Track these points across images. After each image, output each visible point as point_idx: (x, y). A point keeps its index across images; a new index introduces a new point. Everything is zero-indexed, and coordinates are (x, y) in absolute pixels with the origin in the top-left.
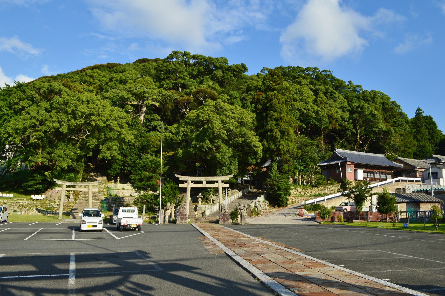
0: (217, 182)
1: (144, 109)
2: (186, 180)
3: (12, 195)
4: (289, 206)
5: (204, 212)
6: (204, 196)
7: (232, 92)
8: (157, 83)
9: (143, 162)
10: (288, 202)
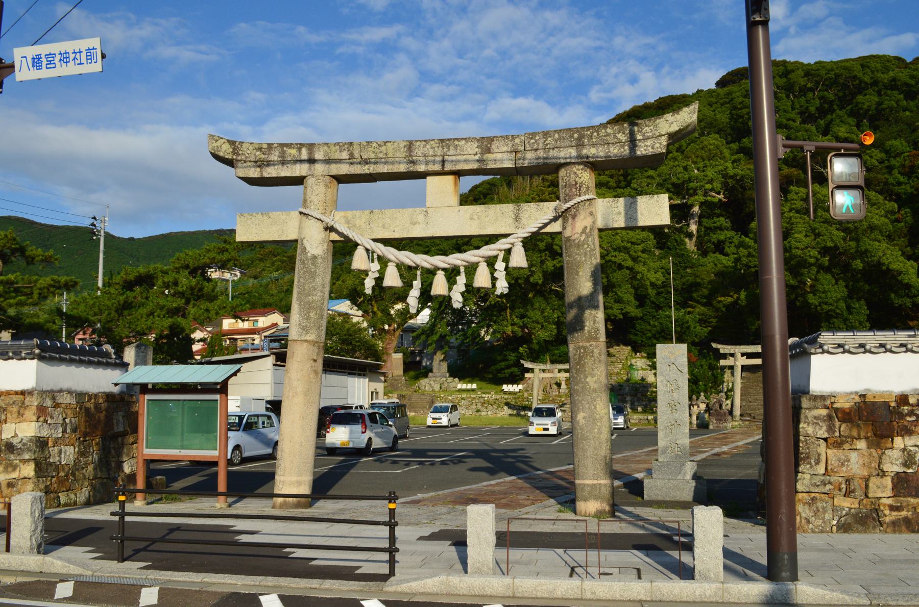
1: (696, 209)
2: (732, 352)
3: (474, 386)
7: (890, 143)
8: (732, 145)
9: (661, 324)
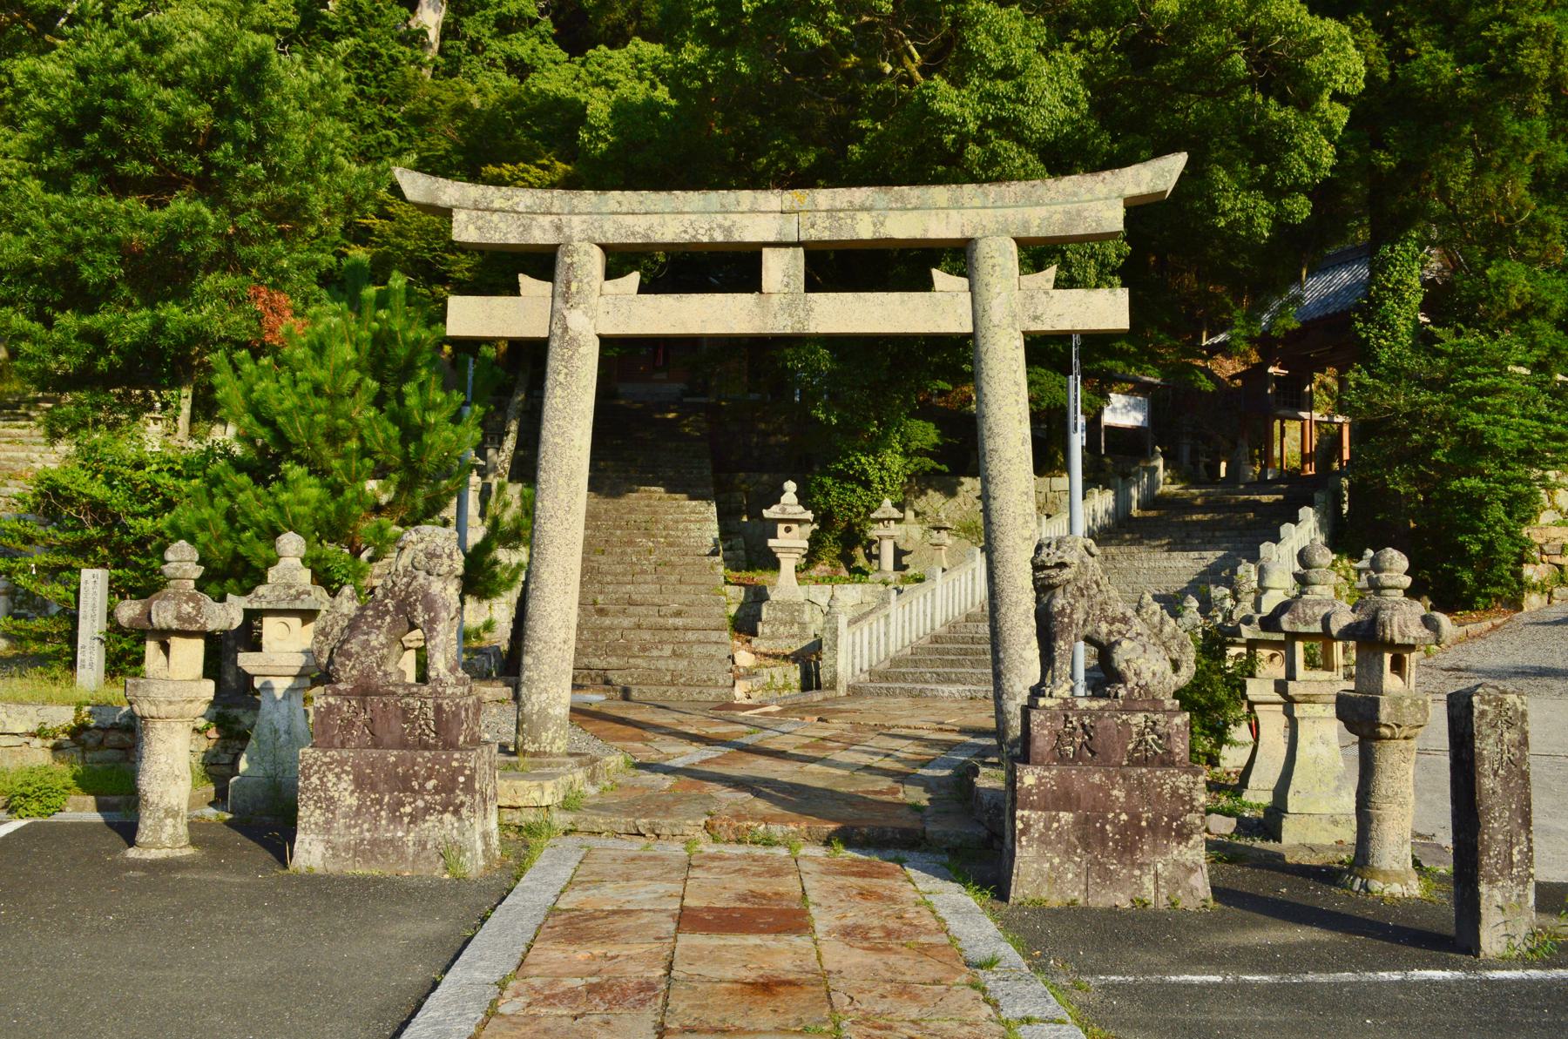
0: (958, 255)
2: (540, 234)
4: (1533, 601)
5: (817, 646)
6: (825, 519)
10: (1528, 570)
